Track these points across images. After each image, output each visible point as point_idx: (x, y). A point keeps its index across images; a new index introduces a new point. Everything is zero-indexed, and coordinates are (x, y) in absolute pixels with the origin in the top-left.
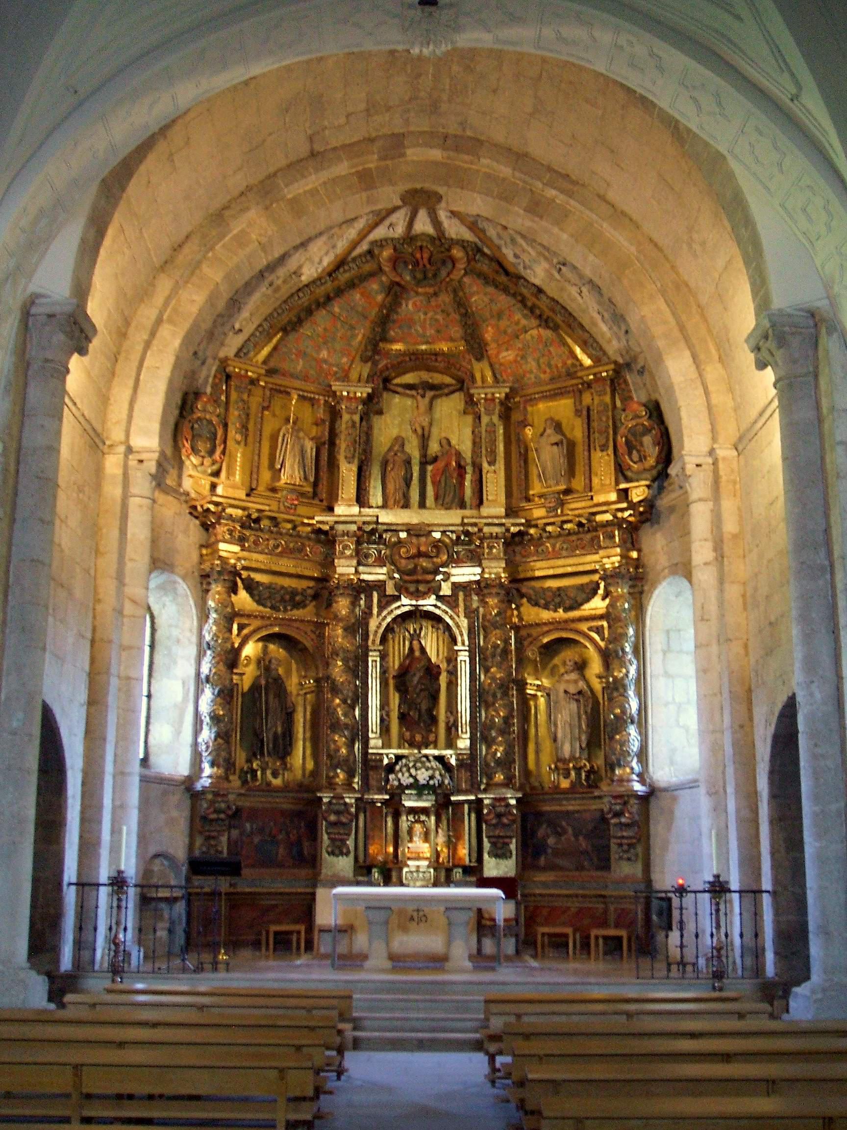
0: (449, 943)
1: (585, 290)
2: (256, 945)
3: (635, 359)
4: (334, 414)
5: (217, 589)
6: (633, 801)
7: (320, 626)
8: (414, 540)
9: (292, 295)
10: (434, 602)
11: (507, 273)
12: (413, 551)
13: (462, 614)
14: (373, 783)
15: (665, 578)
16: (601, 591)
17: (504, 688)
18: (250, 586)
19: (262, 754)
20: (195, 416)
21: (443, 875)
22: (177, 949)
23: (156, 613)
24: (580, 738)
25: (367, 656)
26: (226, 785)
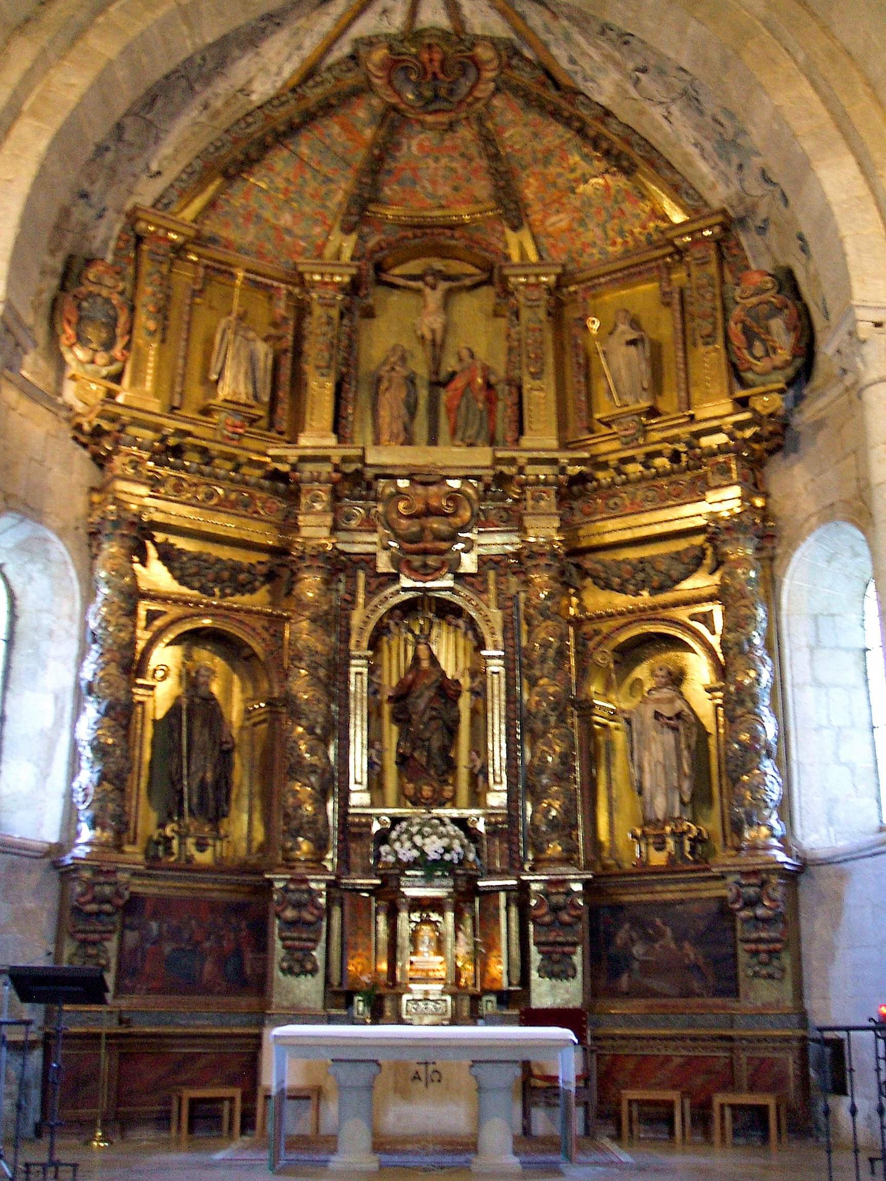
0: (479, 1119)
1: (675, 109)
2: (163, 1121)
3: (752, 210)
4: (302, 310)
5: (111, 549)
6: (775, 880)
7: (276, 622)
8: (420, 490)
9: (238, 121)
10: (450, 583)
11: (557, 86)
12: (419, 506)
13: (493, 604)
14: (355, 859)
15: (811, 530)
16: (708, 561)
17: (560, 707)
18: (168, 556)
19: (181, 814)
20: (83, 289)
21: (466, 1004)
22: (29, 1130)
23: (17, 591)
24: (680, 787)
25: (348, 665)
26: (114, 856)
